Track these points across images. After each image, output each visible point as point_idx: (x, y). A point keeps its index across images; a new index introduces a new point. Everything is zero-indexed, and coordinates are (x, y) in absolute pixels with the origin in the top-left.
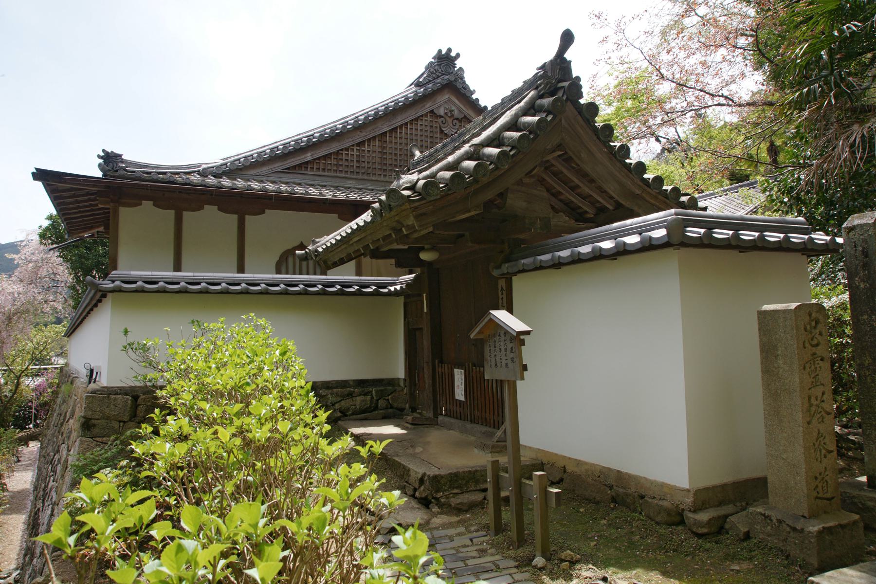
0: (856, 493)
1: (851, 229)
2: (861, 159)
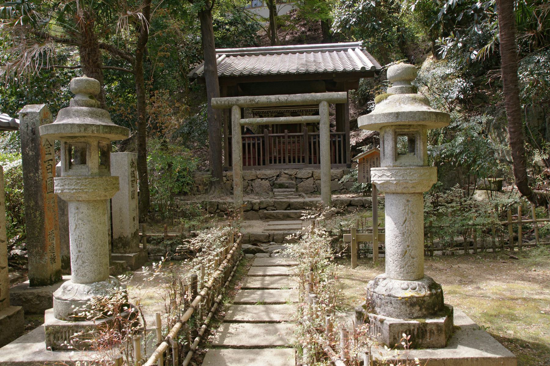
0: (21, 292)
1: (25, 115)
2: (38, 68)
